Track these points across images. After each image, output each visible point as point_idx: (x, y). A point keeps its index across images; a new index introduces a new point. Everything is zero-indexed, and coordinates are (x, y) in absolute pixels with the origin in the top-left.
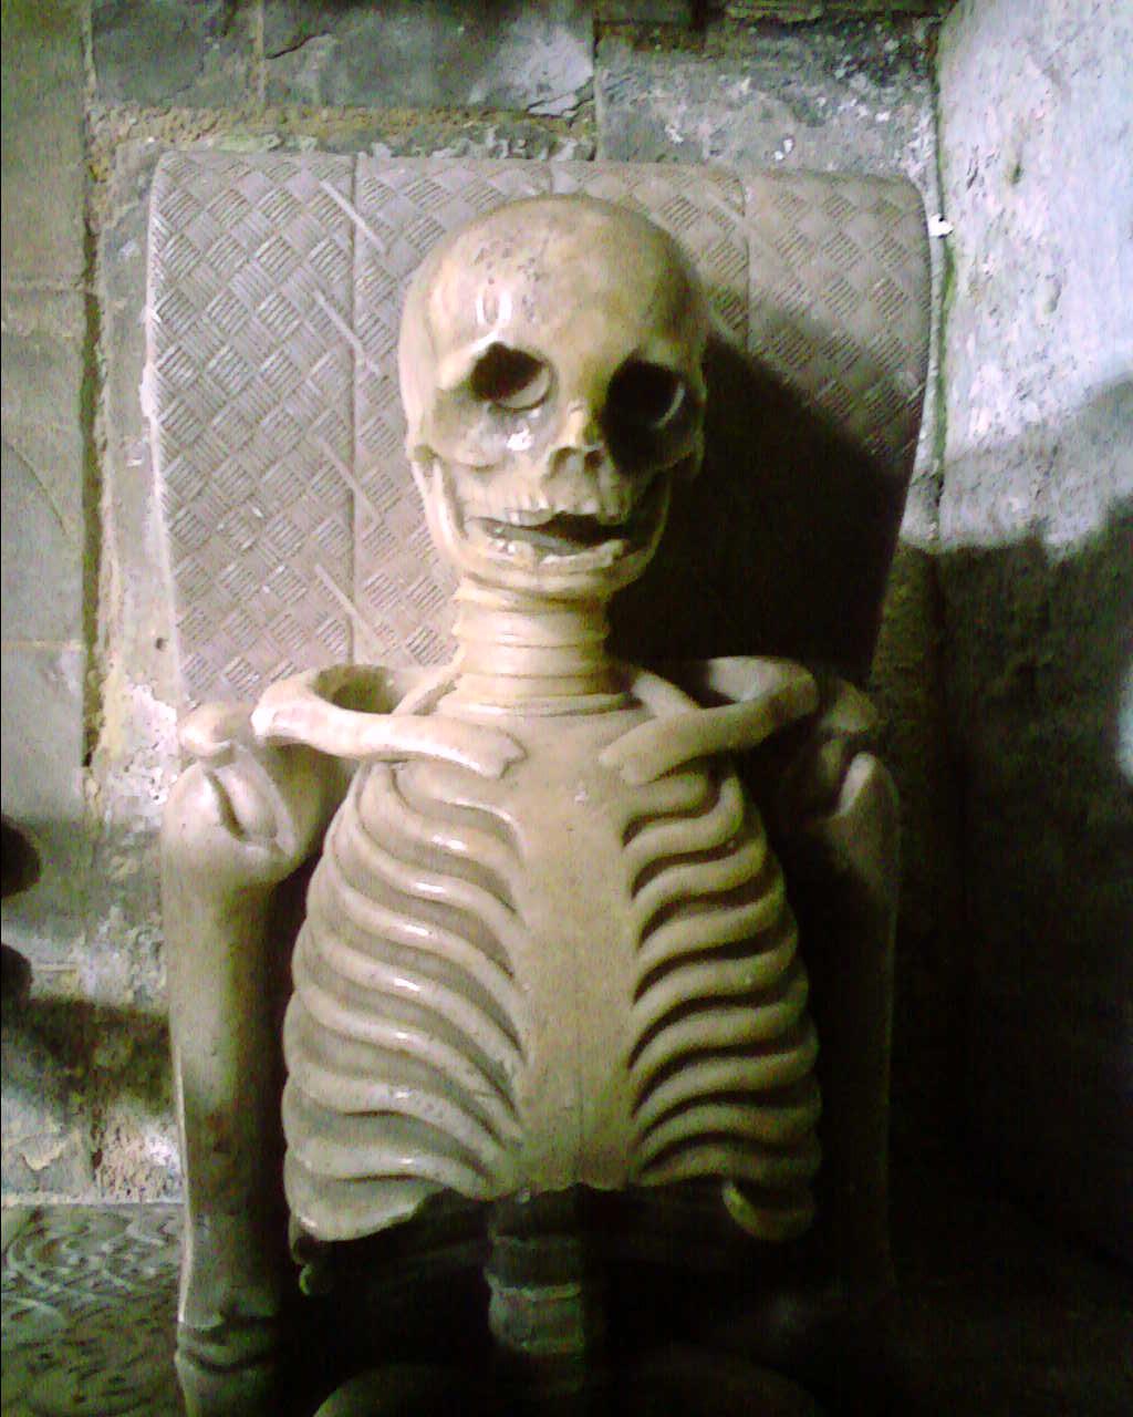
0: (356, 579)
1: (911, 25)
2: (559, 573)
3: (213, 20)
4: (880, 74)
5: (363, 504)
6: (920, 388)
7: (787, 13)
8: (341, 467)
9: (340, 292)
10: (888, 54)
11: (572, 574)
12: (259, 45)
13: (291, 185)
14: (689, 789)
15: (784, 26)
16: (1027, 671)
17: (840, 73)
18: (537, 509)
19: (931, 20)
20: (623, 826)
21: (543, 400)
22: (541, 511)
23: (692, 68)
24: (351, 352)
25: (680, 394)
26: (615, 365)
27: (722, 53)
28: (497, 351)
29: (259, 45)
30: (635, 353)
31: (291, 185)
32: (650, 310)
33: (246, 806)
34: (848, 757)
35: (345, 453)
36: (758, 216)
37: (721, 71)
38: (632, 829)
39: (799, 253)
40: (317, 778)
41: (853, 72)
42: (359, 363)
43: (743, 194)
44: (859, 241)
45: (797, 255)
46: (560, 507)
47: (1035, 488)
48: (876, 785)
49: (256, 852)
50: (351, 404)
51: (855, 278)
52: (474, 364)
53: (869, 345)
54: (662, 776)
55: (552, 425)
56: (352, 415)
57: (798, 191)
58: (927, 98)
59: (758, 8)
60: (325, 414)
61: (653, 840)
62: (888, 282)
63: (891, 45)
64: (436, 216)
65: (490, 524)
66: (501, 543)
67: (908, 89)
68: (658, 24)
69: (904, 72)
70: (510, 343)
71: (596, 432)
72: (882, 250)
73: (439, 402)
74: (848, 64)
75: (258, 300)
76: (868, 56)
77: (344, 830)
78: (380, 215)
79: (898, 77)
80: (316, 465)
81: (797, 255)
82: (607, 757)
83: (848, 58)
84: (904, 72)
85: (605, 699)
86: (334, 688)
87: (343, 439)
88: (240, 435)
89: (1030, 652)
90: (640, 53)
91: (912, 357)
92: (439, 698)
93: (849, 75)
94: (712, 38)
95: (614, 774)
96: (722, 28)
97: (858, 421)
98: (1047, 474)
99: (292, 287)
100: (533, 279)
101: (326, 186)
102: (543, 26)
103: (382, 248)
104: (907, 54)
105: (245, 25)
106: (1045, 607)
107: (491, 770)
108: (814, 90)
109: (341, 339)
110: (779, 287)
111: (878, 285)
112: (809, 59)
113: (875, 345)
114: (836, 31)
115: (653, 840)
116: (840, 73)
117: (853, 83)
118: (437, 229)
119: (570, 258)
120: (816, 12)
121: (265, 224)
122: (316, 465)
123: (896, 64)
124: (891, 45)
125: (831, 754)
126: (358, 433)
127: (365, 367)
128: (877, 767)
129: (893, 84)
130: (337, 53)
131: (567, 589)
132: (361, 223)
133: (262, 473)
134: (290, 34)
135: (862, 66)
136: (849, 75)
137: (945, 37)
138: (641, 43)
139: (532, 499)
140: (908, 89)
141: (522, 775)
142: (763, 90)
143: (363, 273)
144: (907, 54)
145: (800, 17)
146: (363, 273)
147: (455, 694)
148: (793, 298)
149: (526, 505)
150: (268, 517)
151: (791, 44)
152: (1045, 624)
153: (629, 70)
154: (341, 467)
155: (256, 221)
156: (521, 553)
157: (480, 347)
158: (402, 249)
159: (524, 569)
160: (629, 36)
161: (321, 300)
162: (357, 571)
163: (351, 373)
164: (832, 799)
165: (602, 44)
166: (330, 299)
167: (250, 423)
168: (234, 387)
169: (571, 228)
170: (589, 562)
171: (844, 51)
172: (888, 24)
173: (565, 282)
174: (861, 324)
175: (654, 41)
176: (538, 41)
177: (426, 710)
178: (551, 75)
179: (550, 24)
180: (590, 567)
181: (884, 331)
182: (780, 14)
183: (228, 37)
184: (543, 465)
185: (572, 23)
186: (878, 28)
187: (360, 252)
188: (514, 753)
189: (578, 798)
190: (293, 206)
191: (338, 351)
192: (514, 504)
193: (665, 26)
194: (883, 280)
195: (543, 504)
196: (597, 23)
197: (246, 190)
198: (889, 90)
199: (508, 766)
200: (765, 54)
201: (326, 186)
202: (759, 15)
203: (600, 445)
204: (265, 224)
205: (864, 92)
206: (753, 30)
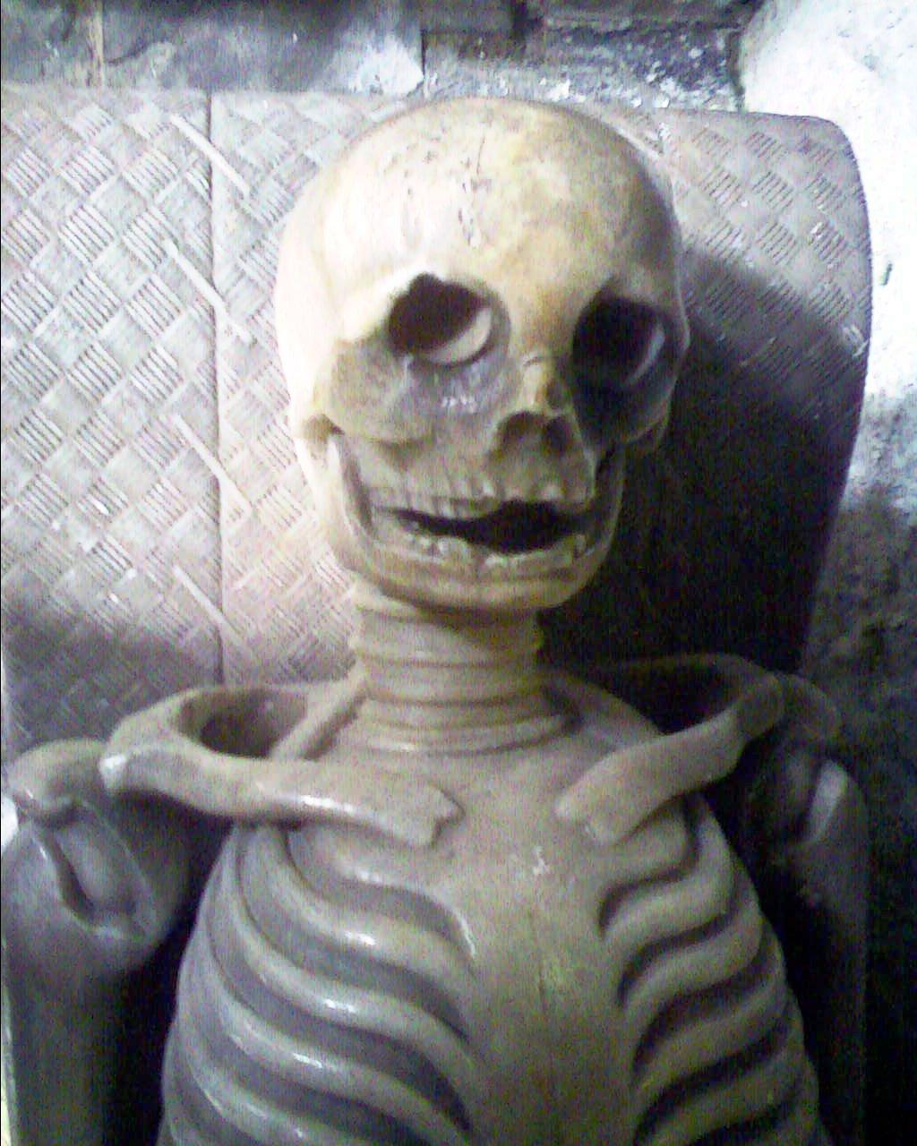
0: (224, 581)
1: (713, 35)
2: (506, 577)
3: (53, 27)
4: (686, 79)
5: (230, 496)
6: (864, 345)
7: (600, 23)
8: (202, 450)
9: (196, 242)
10: (692, 61)
11: (522, 578)
12: (99, 51)
13: (134, 120)
14: (664, 846)
15: (597, 36)
16: (876, 633)
17: (651, 78)
18: (478, 498)
19: (729, 31)
20: (595, 910)
21: (484, 351)
22: (486, 500)
23: (516, 73)
24: (212, 314)
25: (656, 343)
26: (580, 305)
27: (542, 60)
28: (424, 288)
29: (99, 51)
30: (614, 282)
31: (134, 120)
32: (625, 231)
33: (95, 873)
34: (815, 774)
35: (206, 434)
36: (678, 154)
37: (541, 76)
38: (610, 905)
39: (727, 194)
40: (184, 840)
41: (663, 77)
42: (221, 325)
43: (658, 131)
44: (791, 182)
45: (725, 197)
46: (513, 493)
47: (876, 455)
48: (847, 802)
49: (110, 933)
50: (214, 376)
51: (791, 222)
52: (391, 304)
53: (811, 297)
54: (637, 829)
55: (501, 381)
56: (215, 388)
57: (721, 131)
58: (732, 99)
59: (573, 19)
60: (182, 389)
61: (637, 919)
62: (826, 226)
63: (695, 53)
64: (309, 153)
65: (409, 517)
66: (425, 542)
67: (712, 92)
68: (481, 34)
69: (708, 78)
70: (442, 274)
71: (564, 391)
72: (816, 191)
73: (342, 359)
74: (657, 70)
75: (95, 251)
76: (675, 63)
77: (223, 899)
78: (242, 152)
79: (703, 82)
80: (173, 447)
81: (725, 197)
82: (567, 806)
83: (657, 64)
84: (708, 78)
85: (547, 725)
86: (200, 721)
87: (204, 416)
88: (77, 416)
89: (877, 616)
90: (466, 61)
91: (856, 309)
92: (337, 730)
93: (658, 80)
94: (531, 46)
95: (578, 828)
96: (540, 39)
97: (797, 386)
98: (888, 441)
99: (139, 241)
100: (469, 187)
101: (176, 120)
102: (373, 34)
103: (246, 190)
104: (709, 60)
105: (84, 33)
106: (894, 570)
107: (423, 836)
108: (629, 93)
109: (199, 297)
110: (708, 232)
111: (815, 230)
112: (623, 65)
113: (818, 295)
114: (644, 40)
115: (637, 919)
116: (651, 78)
117: (663, 87)
118: (311, 166)
119: (519, 160)
120: (625, 23)
121: (103, 164)
122: (173, 447)
123: (701, 69)
124: (695, 53)
125: (797, 770)
126: (222, 411)
127: (229, 331)
128: (848, 789)
129: (699, 87)
130: (176, 59)
131: (521, 599)
132: (219, 163)
133: (104, 460)
134: (129, 40)
135: (670, 72)
136: (658, 80)
137: (746, 43)
138: (466, 51)
139: (473, 482)
140: (712, 92)
141: (461, 841)
142: (581, 92)
143: (224, 219)
144: (709, 60)
145: (610, 27)
146: (224, 219)
147: (357, 723)
148: (726, 243)
149: (464, 491)
150: (114, 510)
151: (605, 52)
152: (892, 588)
153: (457, 74)
154: (202, 450)
155: (91, 160)
156: (456, 557)
157: (399, 282)
158: (271, 192)
159: (460, 576)
160: (456, 45)
161: (172, 250)
162: (225, 574)
163: (211, 339)
164: (798, 826)
165: (429, 52)
166: (187, 252)
167: (89, 400)
168: (68, 356)
169: (515, 126)
170: (543, 563)
171: (653, 58)
172: (690, 34)
173: (514, 192)
174: (799, 274)
175: (477, 50)
176: (369, 47)
177: (321, 747)
178: (382, 80)
179: (381, 34)
180: (545, 569)
181: (826, 279)
182: (594, 25)
183: (69, 45)
184: (488, 437)
185: (402, 32)
186: (683, 38)
187: (220, 193)
188: (446, 810)
189: (536, 871)
190: (138, 144)
191: (196, 312)
192: (444, 489)
193: (488, 35)
194: (820, 224)
195: (488, 490)
196: (424, 33)
197: (79, 124)
198: (697, 93)
199: (442, 829)
200: (581, 60)
201: (176, 120)
202: (574, 25)
203: (569, 412)
204: (103, 164)
205: (673, 94)
206: (569, 40)
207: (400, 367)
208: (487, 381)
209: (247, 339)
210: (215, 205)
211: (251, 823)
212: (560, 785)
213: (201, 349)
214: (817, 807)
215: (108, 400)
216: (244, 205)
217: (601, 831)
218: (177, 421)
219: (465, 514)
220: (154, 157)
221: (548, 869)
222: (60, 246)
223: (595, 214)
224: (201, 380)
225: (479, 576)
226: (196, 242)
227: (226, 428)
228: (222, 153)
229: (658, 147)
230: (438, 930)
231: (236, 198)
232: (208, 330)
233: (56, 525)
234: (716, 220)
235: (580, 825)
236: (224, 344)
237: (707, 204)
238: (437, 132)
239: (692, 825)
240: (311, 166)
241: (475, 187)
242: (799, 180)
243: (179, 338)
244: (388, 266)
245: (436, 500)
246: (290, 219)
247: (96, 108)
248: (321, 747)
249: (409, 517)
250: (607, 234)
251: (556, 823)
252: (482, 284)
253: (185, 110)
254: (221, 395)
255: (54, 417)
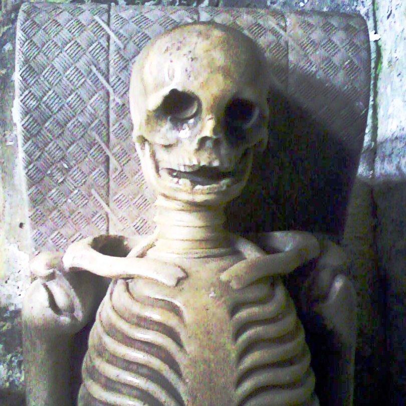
5: (113, 163)
8: (103, 146)
9: (103, 66)
11: (208, 194)
14: (260, 291)
18: (192, 164)
22: (194, 165)
24: (108, 93)
25: (256, 113)
26: (227, 99)
31: (81, 18)
33: (61, 301)
35: (105, 139)
42: (111, 98)
43: (286, 22)
44: (338, 43)
45: (310, 50)
50: (108, 117)
55: (199, 125)
60: (96, 121)
61: (243, 314)
62: (352, 61)
64: (146, 32)
65: (171, 171)
70: (180, 89)
71: (219, 129)
72: (348, 47)
77: (105, 310)
78: (121, 31)
81: (310, 50)
82: (224, 277)
88: (57, 131)
100: (190, 60)
101: (97, 18)
103: (122, 46)
107: (173, 283)
109: (103, 88)
110: (302, 64)
111: (347, 63)
118: (147, 38)
121: (69, 35)
125: (325, 276)
126: (111, 130)
127: (114, 100)
132: (112, 35)
133: (67, 148)
139: (190, 160)
141: (185, 285)
143: (113, 57)
149: (188, 163)
150: (71, 168)
154: (103, 146)
155: (65, 34)
157: (166, 91)
158: (131, 47)
161: (94, 69)
162: (111, 192)
163: (108, 103)
164: (325, 297)
166: (99, 69)
167: (62, 125)
168: (55, 109)
169: (208, 37)
170: (216, 188)
173: (205, 62)
177: (142, 255)
187: (112, 48)
188: (182, 275)
190: (82, 27)
192: (182, 162)
195: (195, 163)
199: (179, 281)
201: (97, 18)
203: (221, 135)
204: (69, 35)
207: (167, 119)
208: (195, 124)
209: (121, 103)
210: (111, 52)
211: (116, 279)
212: (223, 269)
213: (104, 107)
214: (333, 290)
215: (69, 125)
216: (122, 52)
217: (234, 285)
218: (94, 134)
219: (188, 170)
220: (88, 34)
221: (215, 295)
222: (53, 67)
223: (232, 69)
224: (103, 119)
225: (192, 192)
226: (103, 66)
227: (112, 136)
228: (113, 31)
229: (285, 29)
230: (251, 394)
231: (118, 50)
232: (107, 100)
233: (49, 172)
234: (306, 58)
235: (229, 282)
236: (112, 105)
237: (302, 53)
238: (181, 39)
239: (273, 285)
240: (147, 38)
241: (192, 60)
242: (342, 42)
243: (94, 102)
244: (163, 85)
245: (179, 165)
246: (137, 58)
247: (67, 13)
248: (142, 255)
249: (171, 171)
250: (236, 76)
251: (220, 282)
252: (193, 93)
253: (100, 13)
254: (111, 125)
255: (49, 131)
